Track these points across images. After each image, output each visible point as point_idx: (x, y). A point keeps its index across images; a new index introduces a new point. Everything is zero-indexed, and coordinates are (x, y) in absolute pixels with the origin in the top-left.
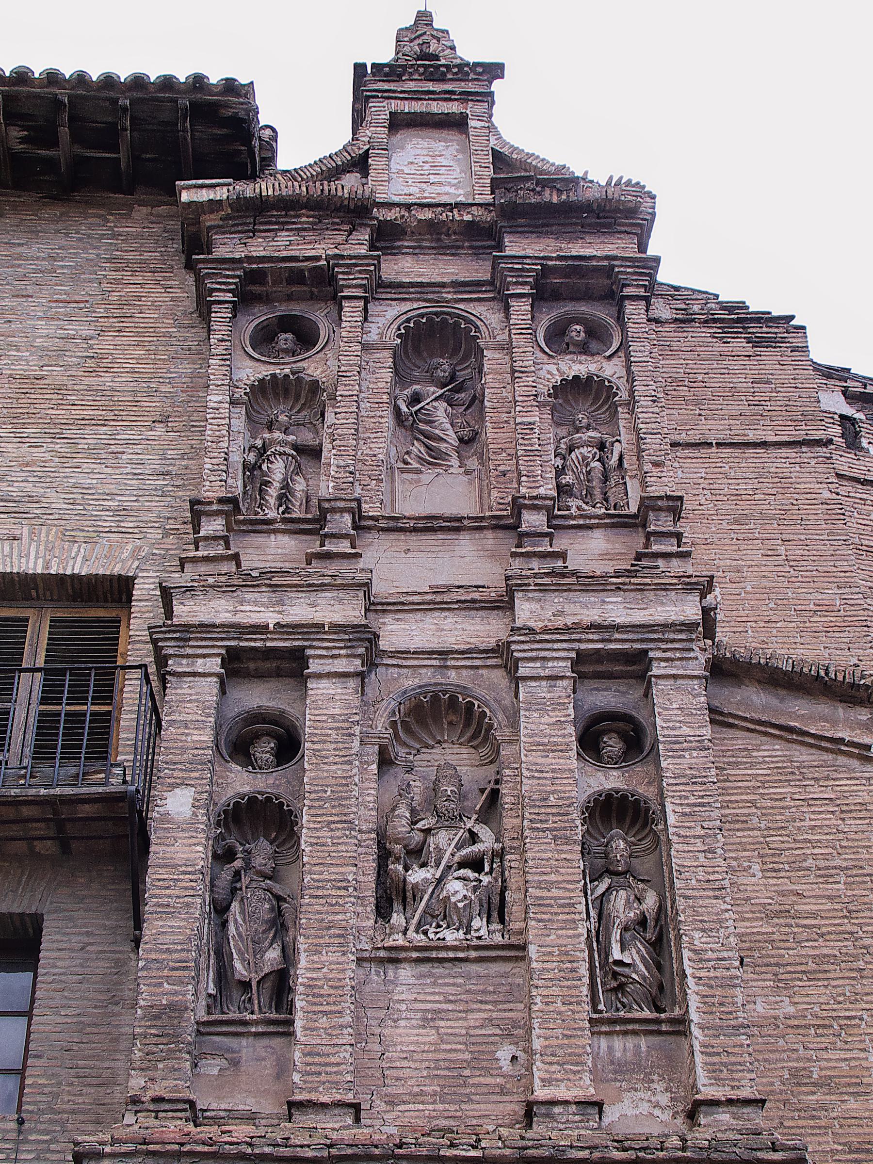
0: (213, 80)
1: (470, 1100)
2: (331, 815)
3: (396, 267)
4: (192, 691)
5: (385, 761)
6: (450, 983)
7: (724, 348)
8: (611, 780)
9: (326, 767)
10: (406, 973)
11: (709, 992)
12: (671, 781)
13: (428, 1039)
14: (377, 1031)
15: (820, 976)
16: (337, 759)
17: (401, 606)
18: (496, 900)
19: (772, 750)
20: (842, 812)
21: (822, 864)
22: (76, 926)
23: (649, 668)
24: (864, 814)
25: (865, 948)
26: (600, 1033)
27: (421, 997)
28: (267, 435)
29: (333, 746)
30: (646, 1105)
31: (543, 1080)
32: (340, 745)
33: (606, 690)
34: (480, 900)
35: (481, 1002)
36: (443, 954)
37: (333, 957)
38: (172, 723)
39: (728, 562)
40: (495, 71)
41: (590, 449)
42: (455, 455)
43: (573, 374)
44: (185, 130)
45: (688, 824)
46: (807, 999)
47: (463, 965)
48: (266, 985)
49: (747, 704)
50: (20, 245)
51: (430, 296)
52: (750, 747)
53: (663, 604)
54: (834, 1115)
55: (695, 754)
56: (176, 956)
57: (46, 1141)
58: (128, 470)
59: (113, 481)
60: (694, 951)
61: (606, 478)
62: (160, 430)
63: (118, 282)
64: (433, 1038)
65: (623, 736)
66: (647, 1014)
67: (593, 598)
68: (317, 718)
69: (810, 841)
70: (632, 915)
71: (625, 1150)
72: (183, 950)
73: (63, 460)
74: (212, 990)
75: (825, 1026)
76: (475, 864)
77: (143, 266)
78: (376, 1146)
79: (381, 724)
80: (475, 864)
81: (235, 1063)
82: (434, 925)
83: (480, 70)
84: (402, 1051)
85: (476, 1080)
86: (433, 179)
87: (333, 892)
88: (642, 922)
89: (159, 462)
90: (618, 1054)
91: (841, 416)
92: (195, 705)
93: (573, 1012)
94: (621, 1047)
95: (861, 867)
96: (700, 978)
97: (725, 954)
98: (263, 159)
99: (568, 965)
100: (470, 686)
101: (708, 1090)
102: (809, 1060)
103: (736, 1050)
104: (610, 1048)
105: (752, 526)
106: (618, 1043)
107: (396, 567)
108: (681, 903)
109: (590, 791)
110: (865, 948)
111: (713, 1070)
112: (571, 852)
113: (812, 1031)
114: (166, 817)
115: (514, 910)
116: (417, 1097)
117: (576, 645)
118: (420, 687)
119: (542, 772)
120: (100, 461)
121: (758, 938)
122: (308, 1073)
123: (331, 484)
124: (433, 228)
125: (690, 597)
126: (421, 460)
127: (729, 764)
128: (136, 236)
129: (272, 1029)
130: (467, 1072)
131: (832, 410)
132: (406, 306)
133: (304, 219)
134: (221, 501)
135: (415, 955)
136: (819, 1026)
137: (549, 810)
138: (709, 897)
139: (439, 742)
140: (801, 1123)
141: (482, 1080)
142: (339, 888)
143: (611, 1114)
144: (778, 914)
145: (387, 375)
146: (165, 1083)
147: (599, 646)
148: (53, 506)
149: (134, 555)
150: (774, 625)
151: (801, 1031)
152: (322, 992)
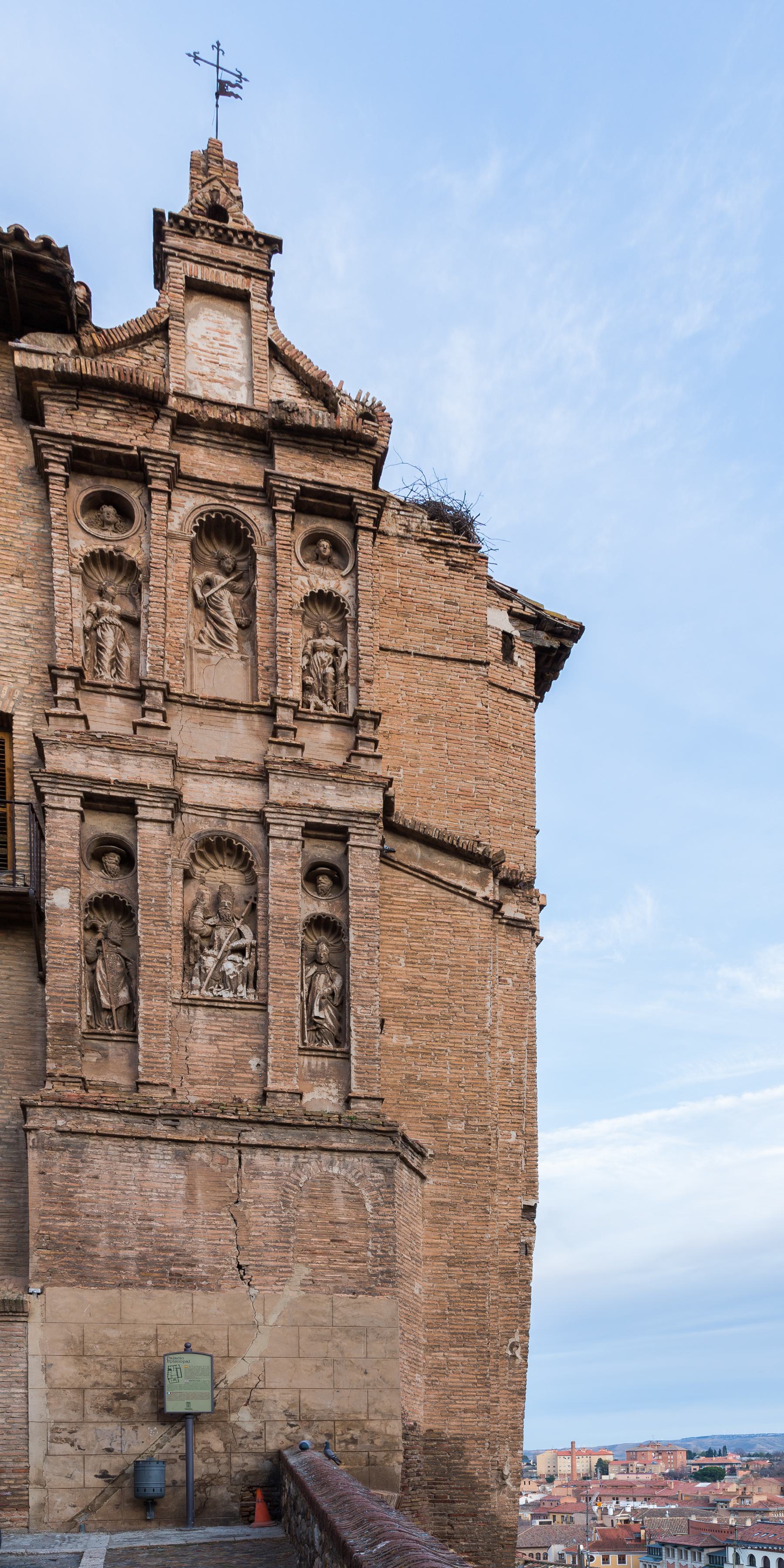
0: (32, 237)
1: (235, 1086)
3: (192, 457)
4: (63, 821)
5: (187, 876)
6: (225, 1020)
8: (321, 907)
9: (151, 884)
10: (200, 1013)
12: (354, 915)
14: (184, 1044)
16: (158, 879)
18: (252, 974)
19: (421, 887)
21: (439, 961)
23: (347, 839)
27: (209, 1027)
28: (99, 603)
29: (155, 870)
32: (160, 870)
33: (322, 847)
34: (243, 975)
36: (221, 1004)
37: (159, 1003)
38: (51, 842)
39: (411, 750)
40: (274, 245)
41: (327, 654)
42: (235, 641)
43: (318, 588)
44: (11, 280)
47: (233, 1011)
49: (410, 854)
51: (219, 494)
53: (360, 794)
55: (369, 899)
56: (67, 995)
61: (336, 678)
62: (17, 585)
64: (215, 1050)
65: (331, 877)
66: (331, 1047)
67: (317, 784)
68: (145, 850)
69: (434, 947)
70: (326, 991)
71: (310, 1120)
72: (71, 992)
74: (89, 1013)
75: (427, 1054)
76: (241, 951)
79: (185, 854)
80: (241, 951)
81: (105, 1056)
85: (238, 1075)
86: (222, 360)
87: (158, 965)
89: (20, 615)
90: (313, 1067)
91: (504, 632)
94: (316, 1062)
97: (373, 1020)
98: (79, 316)
100: (240, 835)
104: (309, 1063)
105: (429, 724)
106: (314, 1061)
107: (197, 737)
108: (352, 989)
109: (309, 913)
111: (360, 1081)
112: (294, 953)
114: (53, 907)
115: (261, 982)
116: (205, 1081)
117: (305, 818)
118: (209, 832)
121: (399, 1001)
123: (148, 665)
126: (212, 641)
127: (394, 893)
129: (125, 1039)
130: (233, 1070)
131: (498, 627)
133: (118, 401)
134: (71, 669)
135: (205, 1003)
136: (424, 1053)
137: (283, 926)
139: (221, 866)
140: (408, 1102)
141: (241, 1075)
142: (161, 962)
143: (307, 1098)
144: (411, 989)
145: (185, 564)
146: (66, 1067)
147: (319, 821)
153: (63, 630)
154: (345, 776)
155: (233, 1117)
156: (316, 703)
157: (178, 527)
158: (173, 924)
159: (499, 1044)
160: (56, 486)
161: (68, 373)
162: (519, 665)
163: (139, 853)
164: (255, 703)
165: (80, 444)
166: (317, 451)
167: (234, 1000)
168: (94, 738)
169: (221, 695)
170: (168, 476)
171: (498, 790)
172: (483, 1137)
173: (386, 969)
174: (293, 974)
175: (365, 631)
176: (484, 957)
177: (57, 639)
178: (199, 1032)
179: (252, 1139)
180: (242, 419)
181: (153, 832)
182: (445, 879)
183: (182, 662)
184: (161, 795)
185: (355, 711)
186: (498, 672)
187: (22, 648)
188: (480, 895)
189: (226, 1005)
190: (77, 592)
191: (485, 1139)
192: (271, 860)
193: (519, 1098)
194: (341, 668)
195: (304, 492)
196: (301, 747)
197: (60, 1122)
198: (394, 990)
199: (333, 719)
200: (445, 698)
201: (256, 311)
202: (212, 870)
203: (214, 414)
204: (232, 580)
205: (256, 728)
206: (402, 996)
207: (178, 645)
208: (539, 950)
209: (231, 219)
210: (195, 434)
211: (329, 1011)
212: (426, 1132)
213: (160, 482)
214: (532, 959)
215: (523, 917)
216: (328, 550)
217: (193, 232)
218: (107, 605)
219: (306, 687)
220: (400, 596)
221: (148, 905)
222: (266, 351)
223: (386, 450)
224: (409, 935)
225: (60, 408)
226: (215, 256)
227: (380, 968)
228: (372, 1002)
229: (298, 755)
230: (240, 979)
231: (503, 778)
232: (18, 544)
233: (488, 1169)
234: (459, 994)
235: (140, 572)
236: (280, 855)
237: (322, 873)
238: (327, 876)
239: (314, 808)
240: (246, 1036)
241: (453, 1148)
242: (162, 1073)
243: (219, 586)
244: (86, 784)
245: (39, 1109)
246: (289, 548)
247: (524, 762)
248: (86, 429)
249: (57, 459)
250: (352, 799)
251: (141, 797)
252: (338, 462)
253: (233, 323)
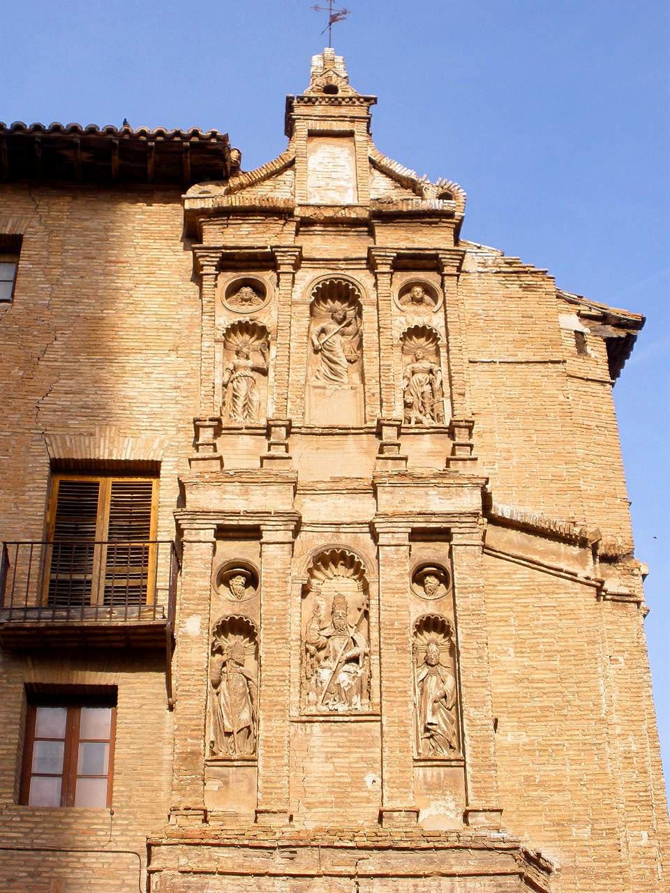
3: (311, 244)
6: (341, 734)
7: (506, 291)
9: (273, 603)
10: (317, 728)
12: (462, 613)
17: (312, 491)
18: (365, 683)
19: (525, 572)
21: (548, 648)
22: (136, 693)
24: (572, 616)
25: (568, 701)
27: (325, 744)
29: (277, 589)
30: (442, 808)
35: (357, 747)
36: (337, 718)
44: (186, 158)
46: (536, 734)
50: (87, 220)
51: (332, 266)
52: (511, 572)
53: (460, 496)
54: (546, 804)
55: (475, 595)
56: (194, 722)
58: (156, 386)
61: (433, 393)
63: (146, 247)
65: (437, 576)
67: (421, 491)
68: (268, 571)
69: (542, 634)
70: (438, 694)
75: (544, 750)
76: (355, 660)
80: (355, 660)
81: (226, 783)
84: (315, 777)
86: (334, 175)
87: (278, 683)
89: (173, 380)
90: (429, 779)
91: (575, 332)
96: (472, 737)
97: (486, 722)
100: (352, 546)
101: (474, 804)
102: (534, 771)
103: (489, 780)
104: (425, 775)
105: (518, 420)
107: (309, 460)
110: (568, 701)
111: (477, 791)
113: (537, 753)
114: (185, 636)
116: (322, 803)
122: (266, 793)
125: (475, 492)
130: (349, 790)
134: (211, 420)
135: (322, 719)
137: (395, 632)
140: (528, 808)
141: (356, 794)
149: (160, 446)
154: (446, 481)
155: (351, 844)
158: (292, 640)
159: (618, 730)
160: (208, 282)
162: (593, 356)
163: (263, 574)
165: (228, 251)
167: (348, 713)
168: (228, 476)
169: (335, 424)
170: (293, 262)
171: (588, 469)
172: (611, 842)
173: (496, 662)
174: (405, 680)
175: (457, 354)
176: (592, 639)
178: (315, 750)
179: (370, 868)
181: (275, 553)
182: (546, 563)
184: (284, 519)
185: (451, 421)
186: (575, 365)
187: (173, 406)
189: (341, 719)
190: (219, 356)
193: (646, 791)
194: (437, 385)
195: (400, 256)
196: (405, 459)
197: (183, 861)
198: (507, 684)
199: (432, 430)
200: (531, 395)
202: (327, 580)
203: (329, 213)
205: (364, 446)
206: (513, 689)
207: (299, 386)
209: (340, 91)
211: (442, 716)
212: (550, 841)
213: (286, 266)
216: (421, 294)
217: (314, 103)
218: (242, 362)
219: (407, 405)
221: (269, 624)
222: (368, 164)
224: (516, 624)
226: (329, 114)
228: (484, 702)
230: (355, 690)
231: (592, 457)
232: (175, 326)
234: (571, 680)
235: (269, 333)
237: (429, 574)
239: (420, 514)
240: (362, 750)
241: (580, 859)
242: (280, 799)
244: (220, 517)
245: (163, 847)
247: (608, 440)
248: (233, 240)
249: (210, 263)
250: (453, 501)
251: (266, 522)
252: (425, 231)
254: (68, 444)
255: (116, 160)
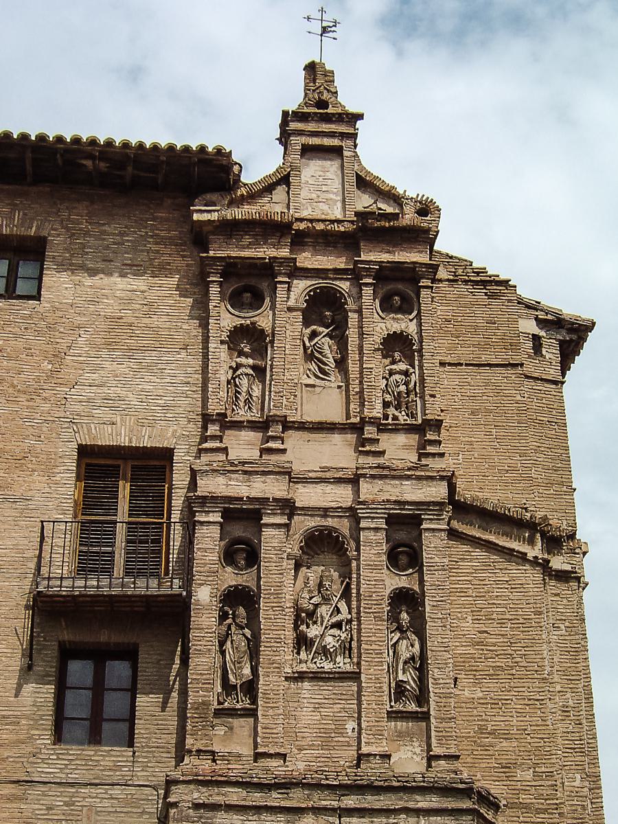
2: (273, 603)
5: (297, 567)
6: (327, 689)
8: (403, 582)
9: (271, 576)
10: (306, 685)
11: (440, 700)
12: (429, 588)
13: (315, 718)
14: (293, 713)
15: (494, 677)
19: (478, 553)
20: (512, 588)
21: (500, 617)
22: (154, 650)
26: (391, 717)
29: (274, 564)
31: (366, 743)
35: (340, 699)
37: (275, 679)
40: (360, 117)
43: (394, 330)
45: (435, 612)
46: (488, 689)
48: (244, 687)
54: (496, 749)
55: (440, 572)
57: (145, 762)
59: (161, 387)
60: (435, 679)
63: (158, 252)
69: (495, 604)
70: (408, 655)
71: (398, 781)
73: (135, 373)
75: (495, 704)
76: (338, 625)
77: (170, 241)
78: (294, 779)
80: (338, 625)
81: (231, 729)
82: (320, 658)
83: (350, 116)
85: (336, 739)
88: (413, 658)
91: (533, 335)
92: (209, 540)
93: (380, 709)
95: (518, 619)
96: (436, 693)
99: (379, 685)
101: (436, 750)
102: (487, 721)
105: (480, 416)
107: (305, 453)
111: (439, 739)
116: (311, 747)
119: (369, 581)
120: (154, 374)
122: (264, 738)
124: (325, 234)
128: (167, 220)
130: (333, 735)
131: (528, 332)
132: (309, 283)
135: (311, 675)
136: (493, 704)
138: (442, 651)
141: (340, 739)
142: (278, 642)
144: (478, 643)
145: (299, 326)
146: (202, 742)
148: (132, 403)
149: (173, 435)
150: (486, 478)
151: (485, 706)
152: (270, 697)
153: (214, 386)
156: (393, 415)
157: (294, 301)
158: (287, 607)
159: (558, 688)
161: (227, 220)
164: (348, 421)
166: (392, 247)
174: (381, 644)
177: (210, 392)
180: (338, 227)
183: (296, 396)
187: (184, 399)
188: (530, 556)
191: (552, 786)
192: (362, 547)
193: (581, 740)
196: (382, 453)
201: (347, 157)
204: (330, 331)
208: (587, 594)
209: (330, 106)
210: (306, 240)
211: (410, 674)
214: (580, 603)
215: (568, 568)
218: (243, 360)
220: (452, 322)
223: (438, 232)
224: (474, 595)
225: (220, 239)
227: (452, 629)
229: (381, 460)
233: (557, 816)
236: (369, 543)
238: (404, 554)
243: (322, 336)
246: (372, 307)
253: (332, 165)
254: (93, 431)
255: (130, 169)
